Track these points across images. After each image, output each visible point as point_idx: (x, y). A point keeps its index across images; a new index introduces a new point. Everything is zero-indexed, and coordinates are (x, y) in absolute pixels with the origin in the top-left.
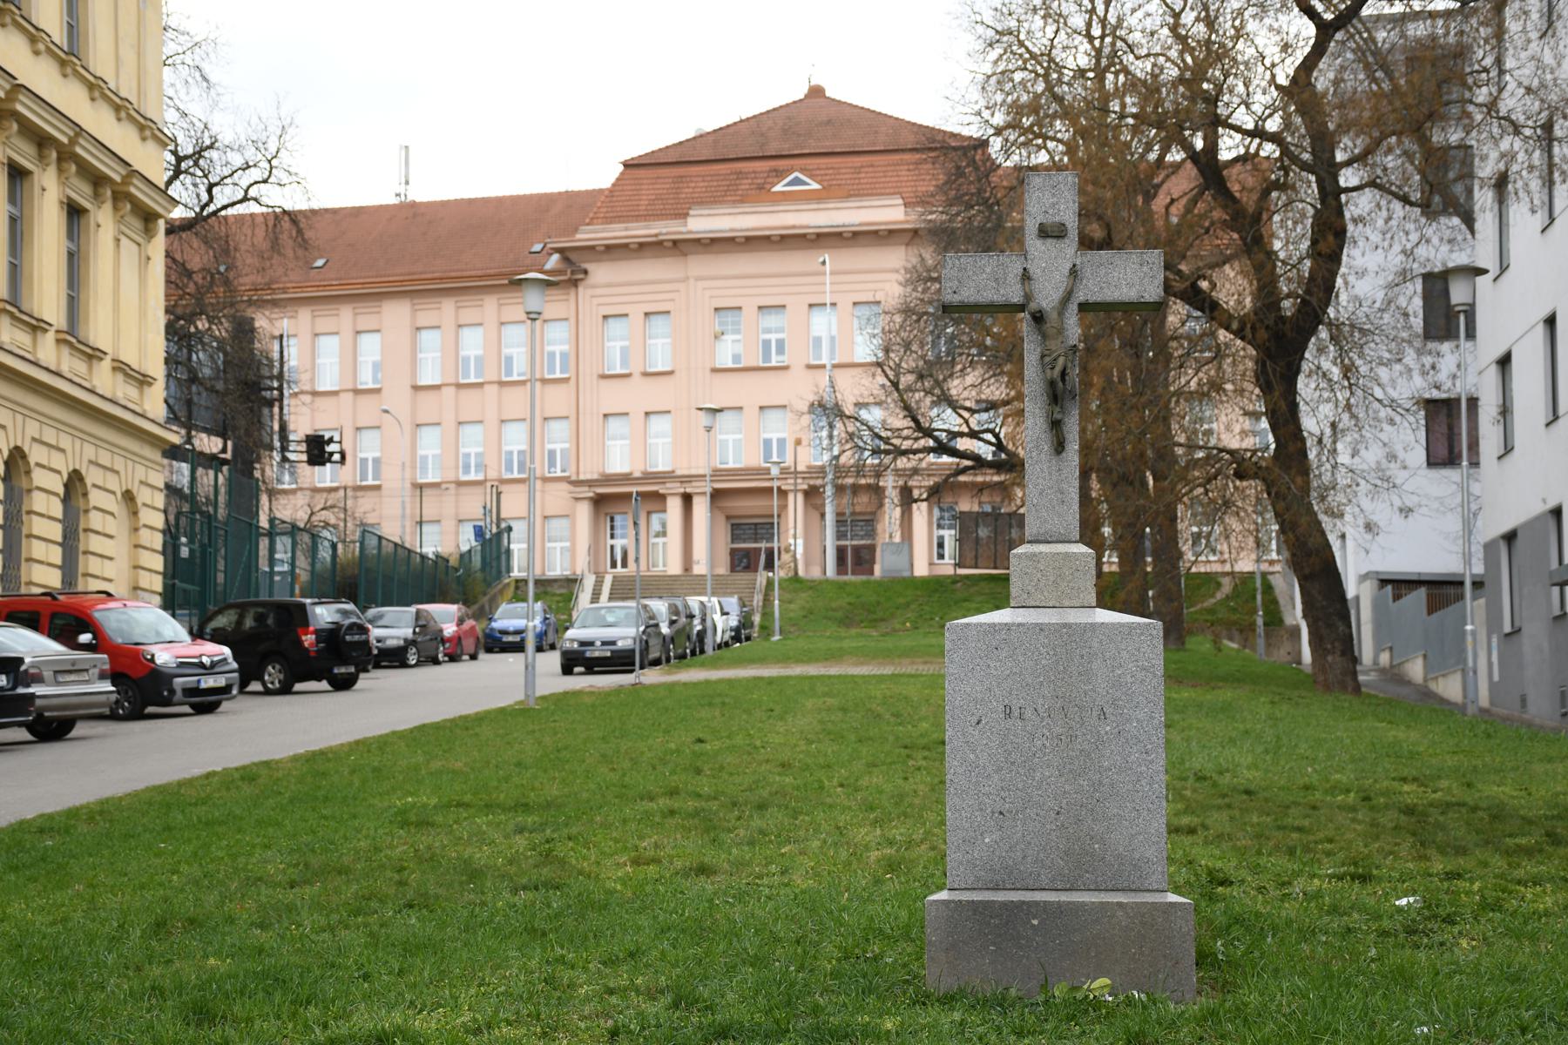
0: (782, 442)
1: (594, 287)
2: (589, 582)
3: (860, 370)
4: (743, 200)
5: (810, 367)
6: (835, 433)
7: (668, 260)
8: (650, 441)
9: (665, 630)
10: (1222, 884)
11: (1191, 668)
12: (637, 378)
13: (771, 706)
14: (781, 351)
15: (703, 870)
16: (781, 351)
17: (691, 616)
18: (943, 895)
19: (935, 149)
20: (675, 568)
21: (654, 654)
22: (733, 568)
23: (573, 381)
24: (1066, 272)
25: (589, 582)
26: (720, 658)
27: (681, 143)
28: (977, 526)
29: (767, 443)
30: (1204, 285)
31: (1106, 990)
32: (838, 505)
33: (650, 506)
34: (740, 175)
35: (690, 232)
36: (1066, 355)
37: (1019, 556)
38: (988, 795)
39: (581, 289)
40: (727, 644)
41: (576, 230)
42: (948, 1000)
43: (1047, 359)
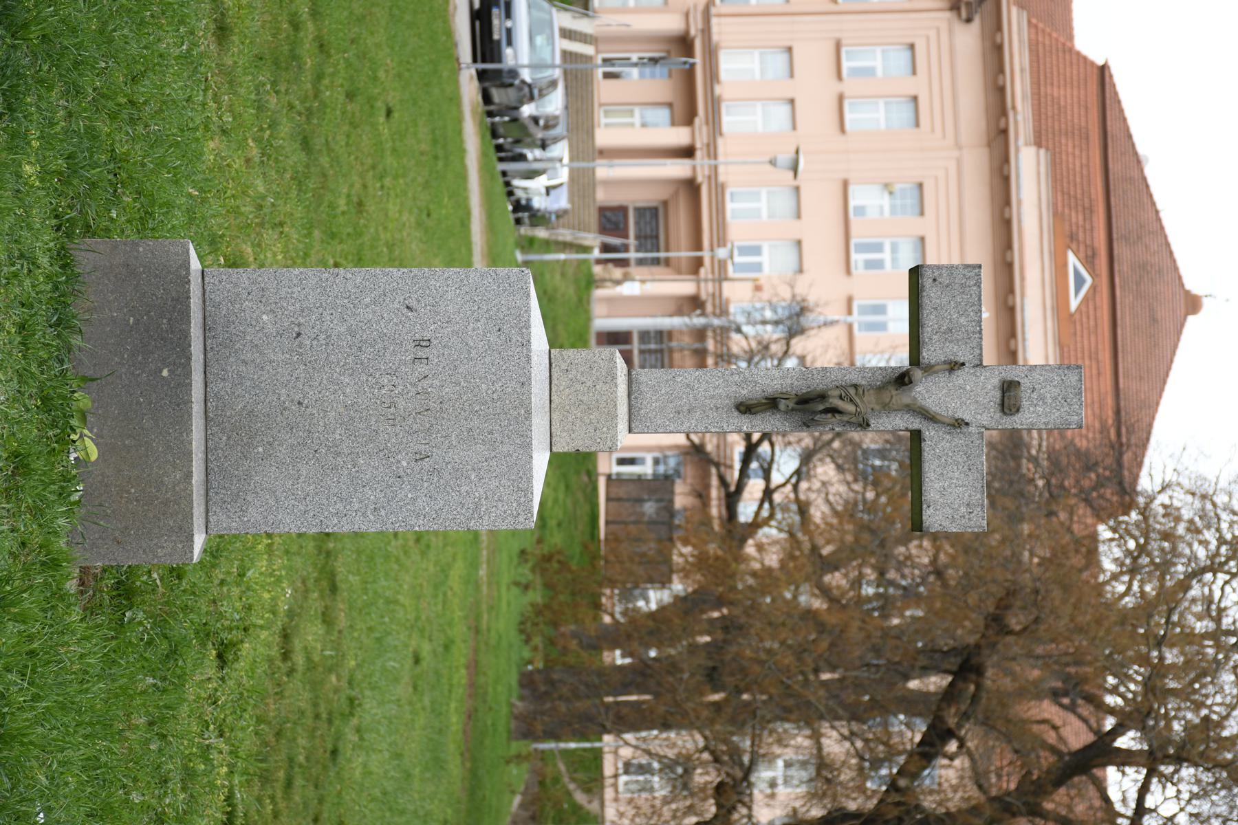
0: (758, 267)
1: (951, 32)
2: (583, 25)
3: (847, 351)
4: (1057, 215)
5: (850, 300)
6: (769, 328)
7: (983, 124)
8: (759, 105)
9: (527, 110)
10: (220, 656)
11: (487, 742)
12: (836, 87)
13: (434, 216)
14: (870, 265)
15: (222, 31)
16: (870, 265)
17: (544, 146)
18: (195, 264)
19: (1119, 434)
20: (604, 137)
21: (497, 95)
22: (603, 211)
23: (832, 7)
24: (959, 415)
25: (583, 25)
26: (492, 177)
27: (1130, 137)
28: (658, 501)
29: (756, 251)
30: (952, 746)
31: (81, 455)
32: (681, 332)
33: (679, 108)
34: (1089, 211)
35: (1017, 150)
36: (857, 414)
37: (612, 360)
38: (320, 318)
39: (948, 14)
40: (510, 194)
41: (1021, 6)
42: (63, 258)
43: (852, 391)
